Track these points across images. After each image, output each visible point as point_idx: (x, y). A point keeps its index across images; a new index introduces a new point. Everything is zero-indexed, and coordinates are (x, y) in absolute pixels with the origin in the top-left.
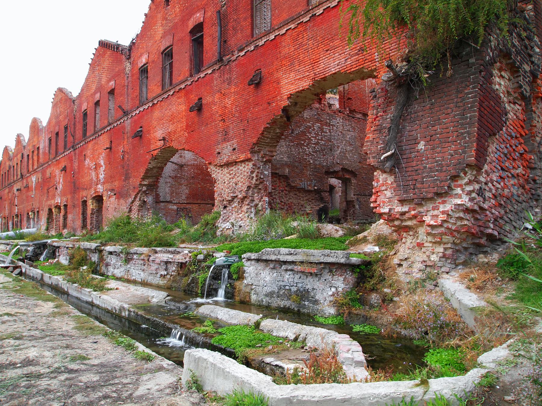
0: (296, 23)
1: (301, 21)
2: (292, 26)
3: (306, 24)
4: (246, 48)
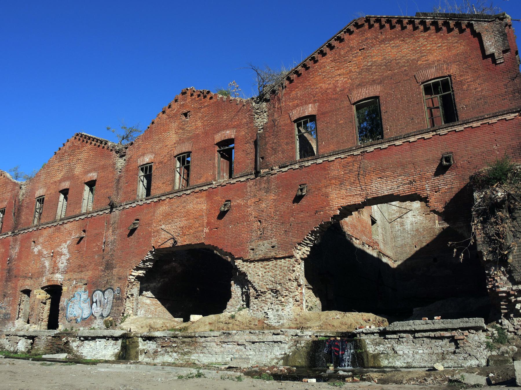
0: (346, 155)
1: (352, 153)
2: (343, 156)
3: (356, 156)
4: (290, 166)
